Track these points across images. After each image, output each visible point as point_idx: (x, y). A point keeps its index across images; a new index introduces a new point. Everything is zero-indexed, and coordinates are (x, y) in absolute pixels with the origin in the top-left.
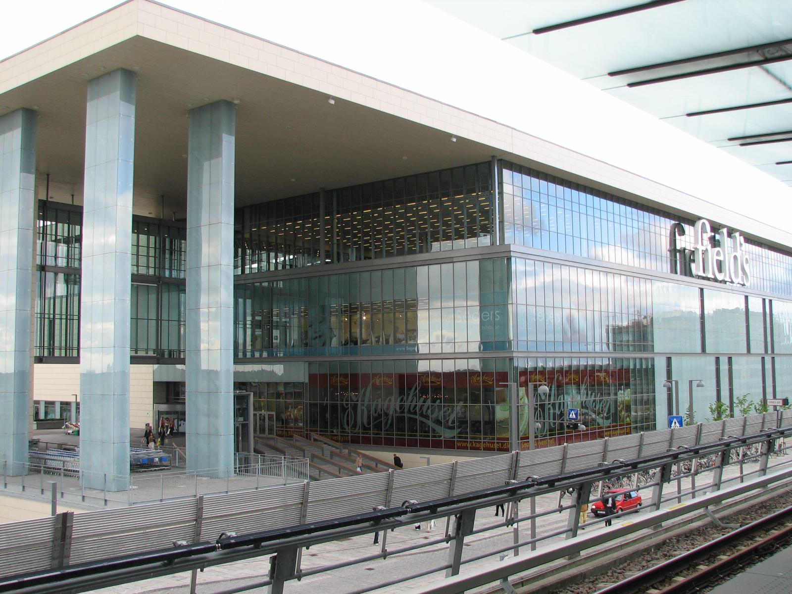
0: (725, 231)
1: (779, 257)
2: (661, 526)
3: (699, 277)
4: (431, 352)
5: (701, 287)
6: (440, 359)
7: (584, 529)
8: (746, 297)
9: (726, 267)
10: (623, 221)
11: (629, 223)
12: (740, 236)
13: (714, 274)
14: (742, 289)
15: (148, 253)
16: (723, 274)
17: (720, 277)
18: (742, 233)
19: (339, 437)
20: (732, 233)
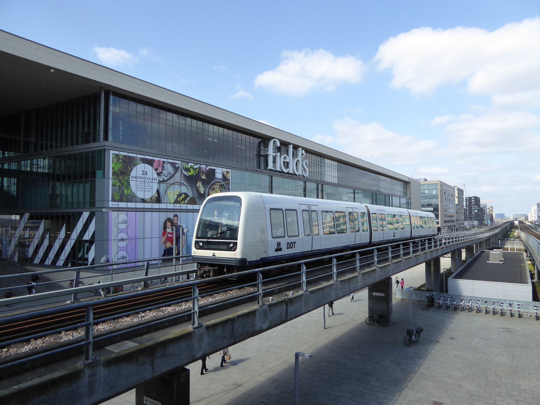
0: (291, 146)
1: (363, 172)
2: (80, 300)
3: (271, 170)
4: (137, 207)
5: (354, 189)
6: (143, 211)
7: (10, 307)
8: (400, 198)
9: (291, 165)
10: (315, 162)
11: (317, 162)
12: (302, 150)
13: (293, 171)
14: (304, 178)
15: (15, 164)
16: (288, 169)
17: (285, 171)
18: (303, 148)
19: (406, 227)
20: (289, 145)
